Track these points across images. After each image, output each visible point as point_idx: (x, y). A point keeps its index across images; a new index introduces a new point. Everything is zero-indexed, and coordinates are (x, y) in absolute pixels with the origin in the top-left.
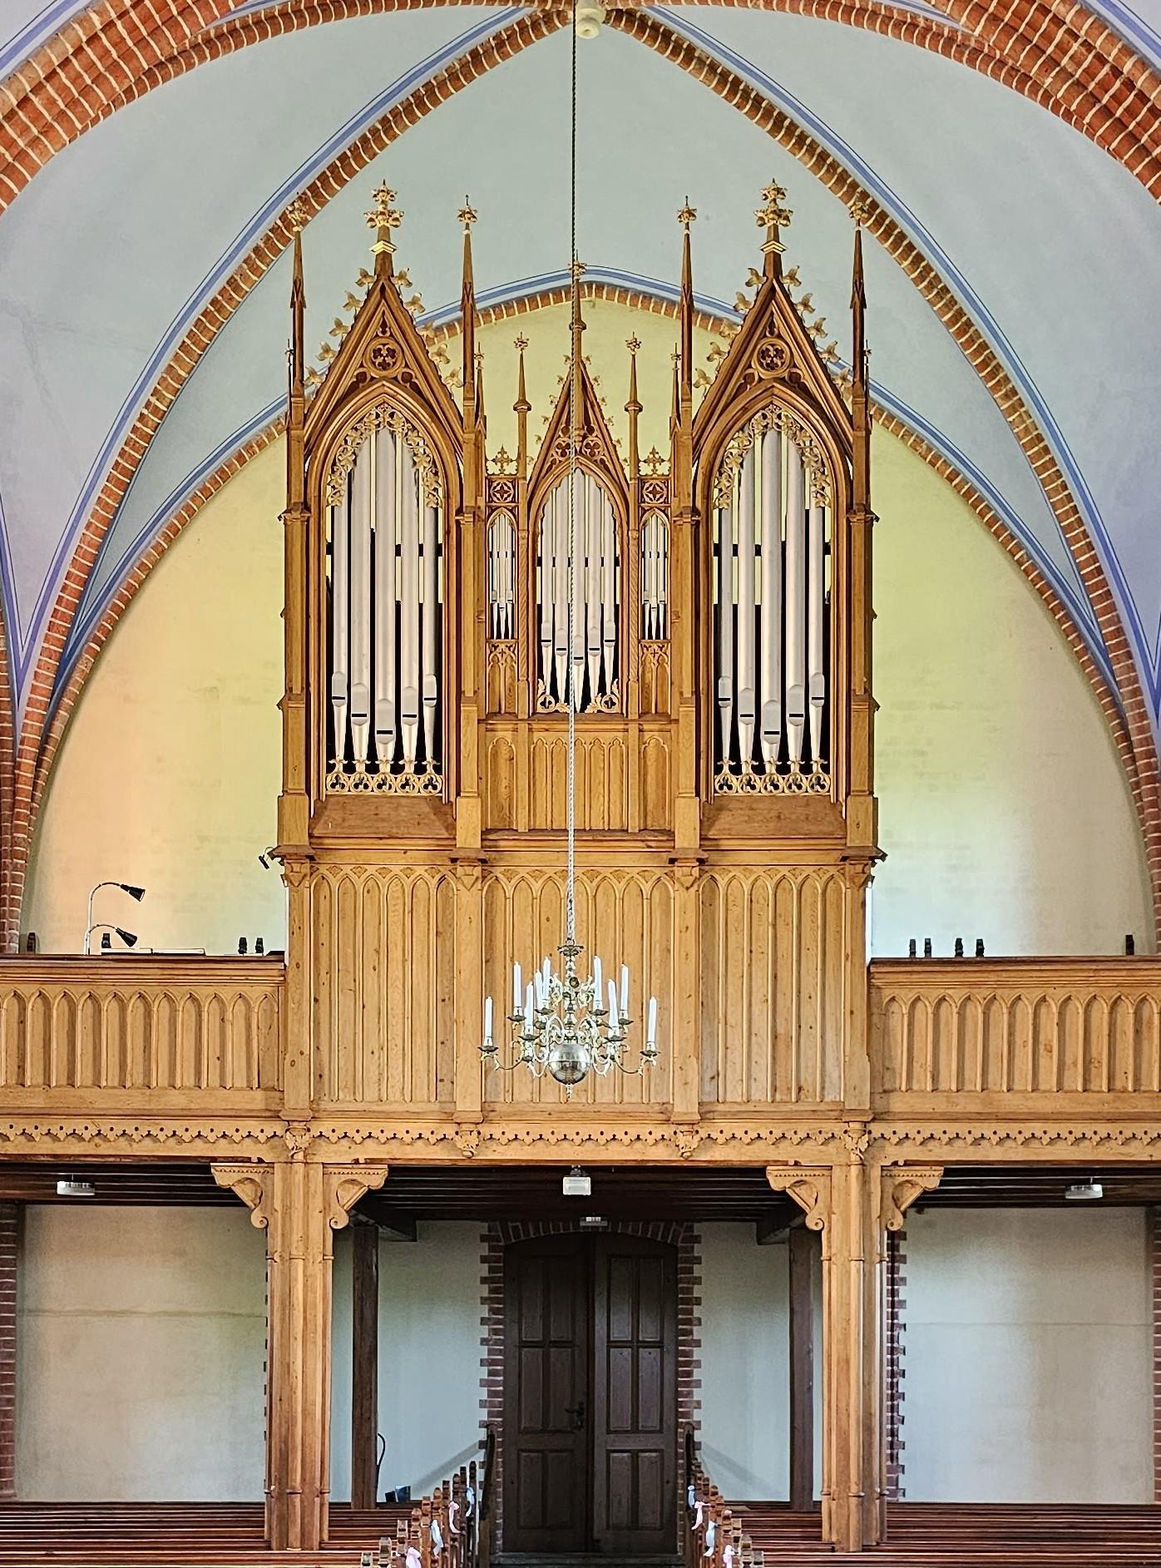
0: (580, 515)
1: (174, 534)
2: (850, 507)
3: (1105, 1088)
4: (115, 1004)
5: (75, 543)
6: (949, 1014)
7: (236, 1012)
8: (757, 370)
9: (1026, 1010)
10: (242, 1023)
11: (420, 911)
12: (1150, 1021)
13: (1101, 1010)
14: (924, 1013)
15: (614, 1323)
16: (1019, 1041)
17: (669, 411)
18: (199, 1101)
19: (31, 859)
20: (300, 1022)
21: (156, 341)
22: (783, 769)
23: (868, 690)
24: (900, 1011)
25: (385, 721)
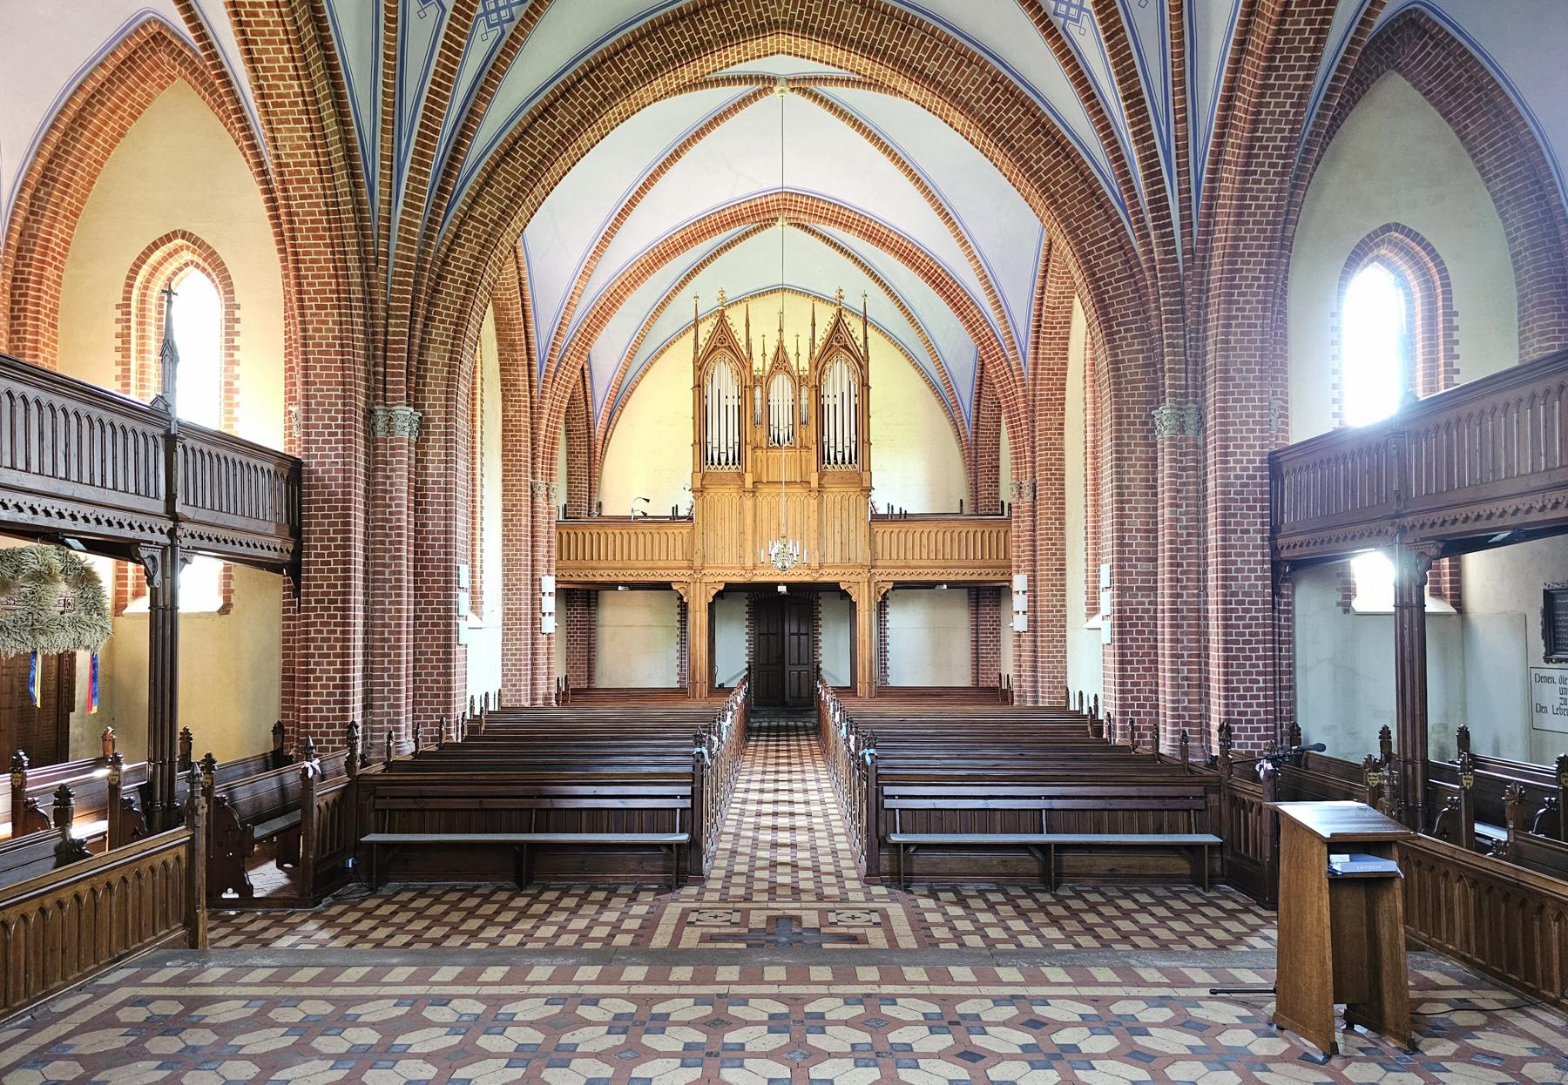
0: (781, 390)
6: (894, 536)
13: (940, 535)
15: (791, 627)
18: (668, 564)
19: (600, 478)
25: (723, 449)
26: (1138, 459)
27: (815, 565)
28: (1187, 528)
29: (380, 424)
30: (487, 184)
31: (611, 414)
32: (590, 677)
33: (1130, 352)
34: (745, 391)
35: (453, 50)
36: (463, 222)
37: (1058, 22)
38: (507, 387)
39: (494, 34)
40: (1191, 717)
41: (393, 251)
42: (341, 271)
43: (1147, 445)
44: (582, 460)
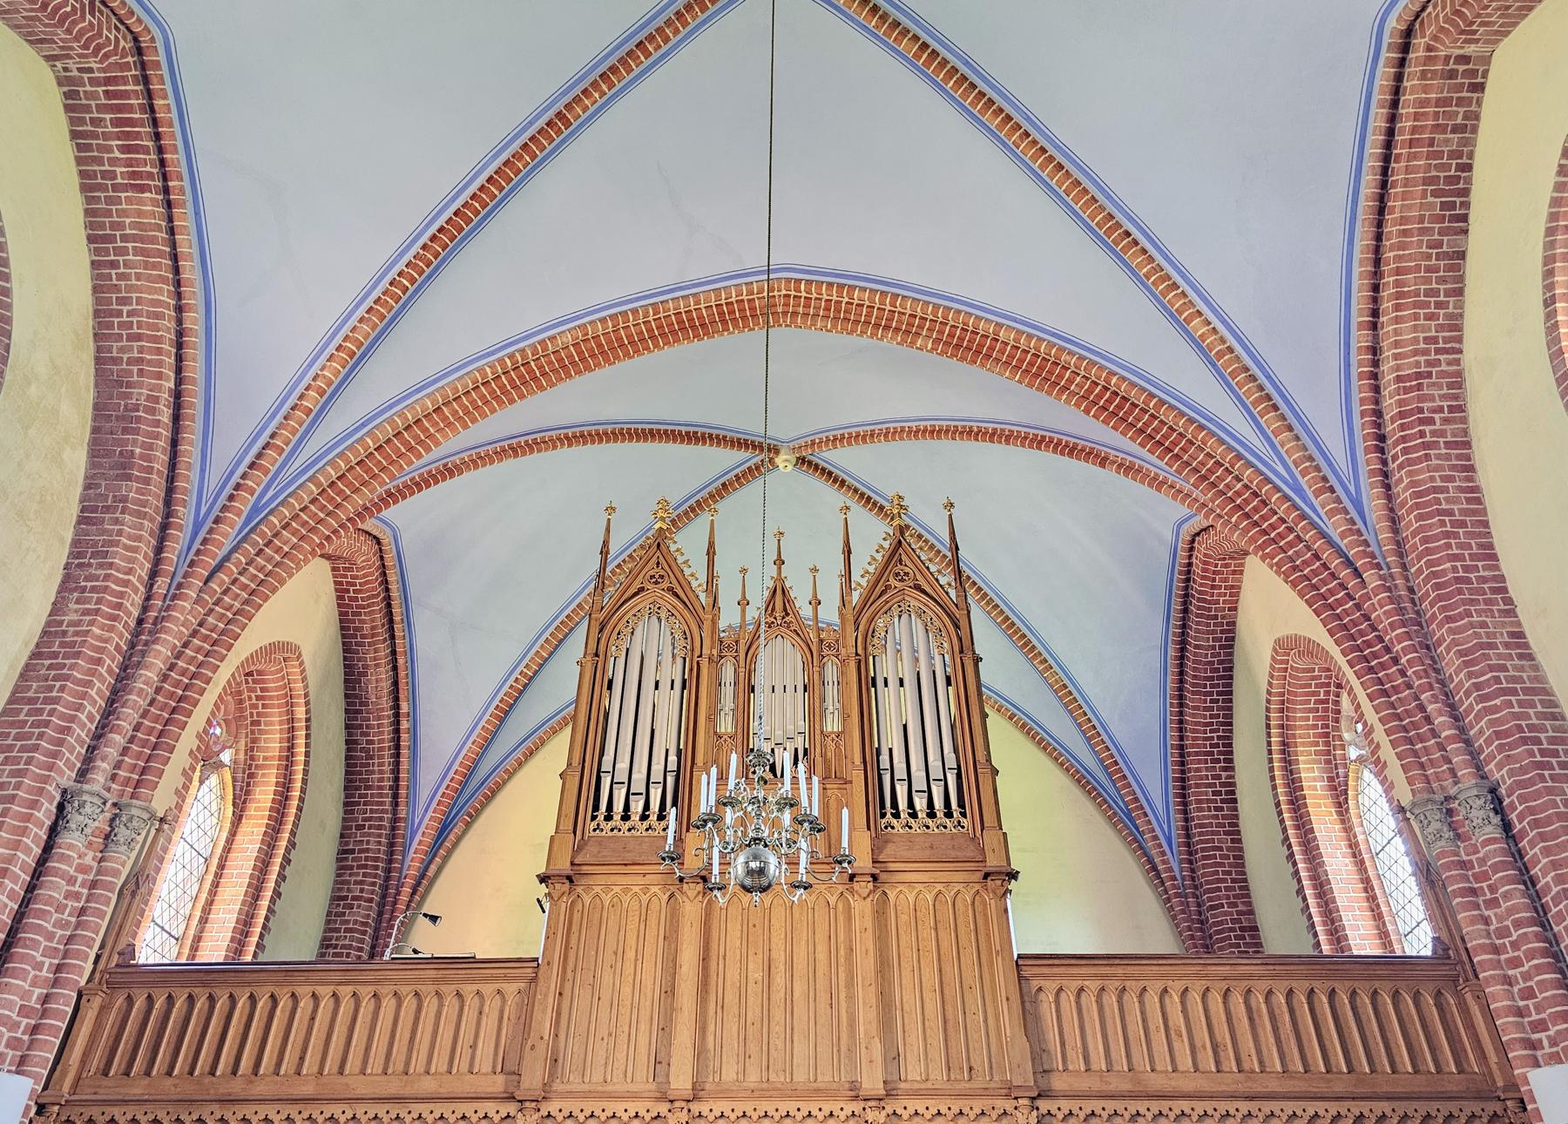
0: (779, 663)
1: (531, 754)
2: (961, 651)
3: (1235, 1069)
4: (393, 1002)
5: (464, 752)
6: (1089, 1000)
7: (492, 1008)
8: (893, 582)
9: (1152, 999)
10: (496, 1014)
11: (652, 922)
12: (1259, 1010)
13: (1216, 1000)
14: (1067, 1001)
16: (1152, 1027)
17: (838, 602)
20: (544, 1011)
21: (532, 636)
22: (932, 814)
23: (989, 760)
24: (1047, 998)
25: (638, 785)
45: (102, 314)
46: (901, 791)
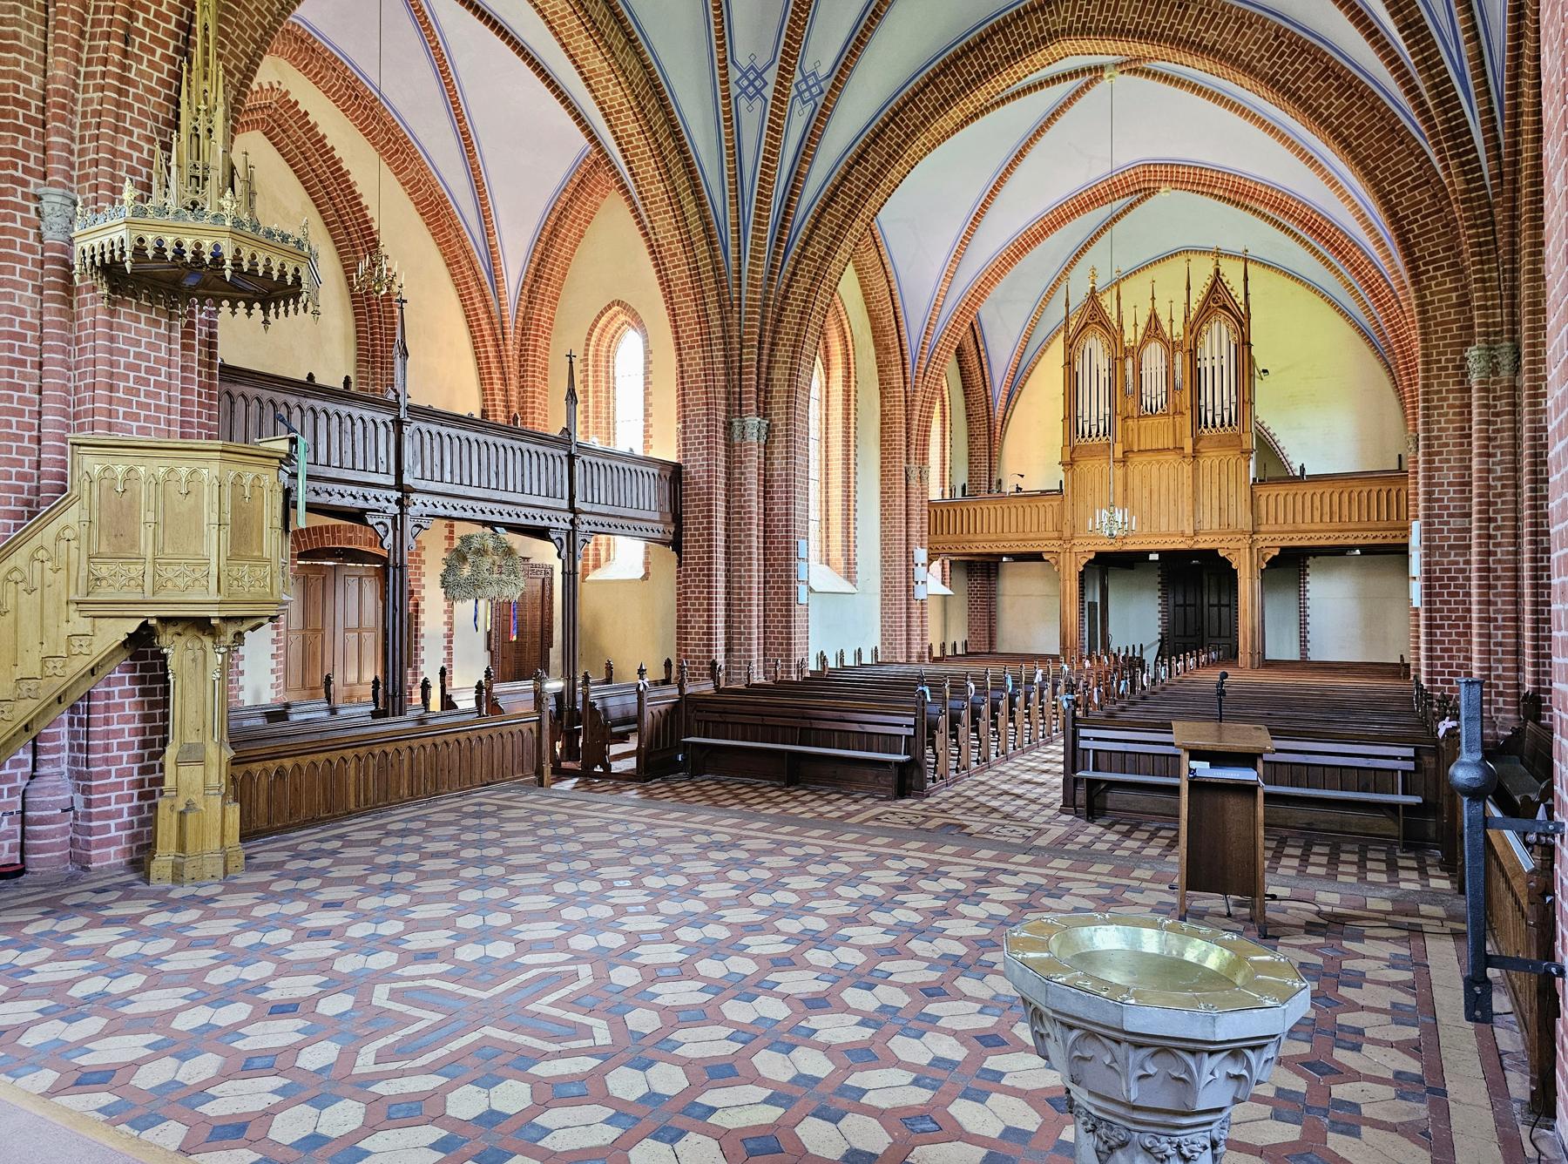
0: (1154, 357)
6: (1299, 498)
13: (1336, 497)
24: (1263, 499)
25: (1094, 422)
26: (1449, 406)
27: (1189, 531)
28: (1500, 478)
29: (737, 432)
30: (817, 227)
31: (1010, 396)
32: (991, 643)
33: (1440, 292)
34: (1116, 363)
35: (775, 130)
36: (798, 262)
37: (826, 85)
38: (884, 384)
39: (808, 108)
40: (1505, 686)
41: (744, 295)
42: (703, 318)
43: (1461, 391)
44: (982, 441)
45: (866, 295)
46: (1210, 415)
